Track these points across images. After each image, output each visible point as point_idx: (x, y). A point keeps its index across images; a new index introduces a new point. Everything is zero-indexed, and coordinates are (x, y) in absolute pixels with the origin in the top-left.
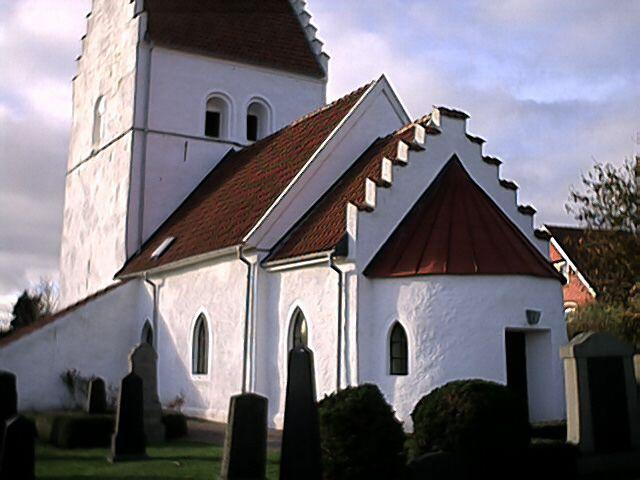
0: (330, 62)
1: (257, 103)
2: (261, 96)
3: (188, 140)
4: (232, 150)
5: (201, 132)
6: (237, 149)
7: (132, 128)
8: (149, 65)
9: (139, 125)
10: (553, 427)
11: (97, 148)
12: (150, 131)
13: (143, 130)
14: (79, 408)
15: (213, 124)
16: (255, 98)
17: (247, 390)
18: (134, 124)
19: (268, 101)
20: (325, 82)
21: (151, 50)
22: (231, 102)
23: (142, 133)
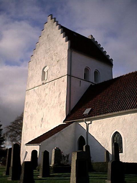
0: (113, 61)
1: (97, 72)
2: (88, 67)
3: (81, 80)
4: (91, 85)
5: (83, 79)
6: (93, 84)
7: (67, 75)
8: (71, 56)
9: (69, 74)
10: (106, 81)
11: (44, 82)
12: (72, 76)
13: (70, 76)
14: (51, 164)
15: (86, 76)
16: (87, 67)
17: (90, 177)
18: (68, 73)
19: (99, 71)
20: (112, 67)
21: (72, 52)
22: (90, 70)
23: (70, 76)
